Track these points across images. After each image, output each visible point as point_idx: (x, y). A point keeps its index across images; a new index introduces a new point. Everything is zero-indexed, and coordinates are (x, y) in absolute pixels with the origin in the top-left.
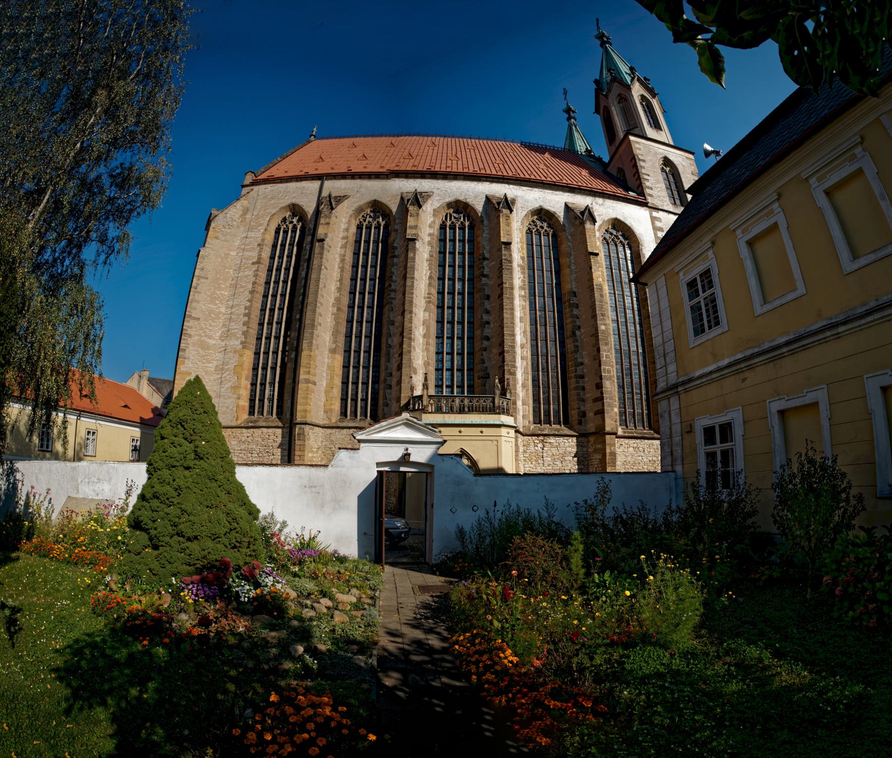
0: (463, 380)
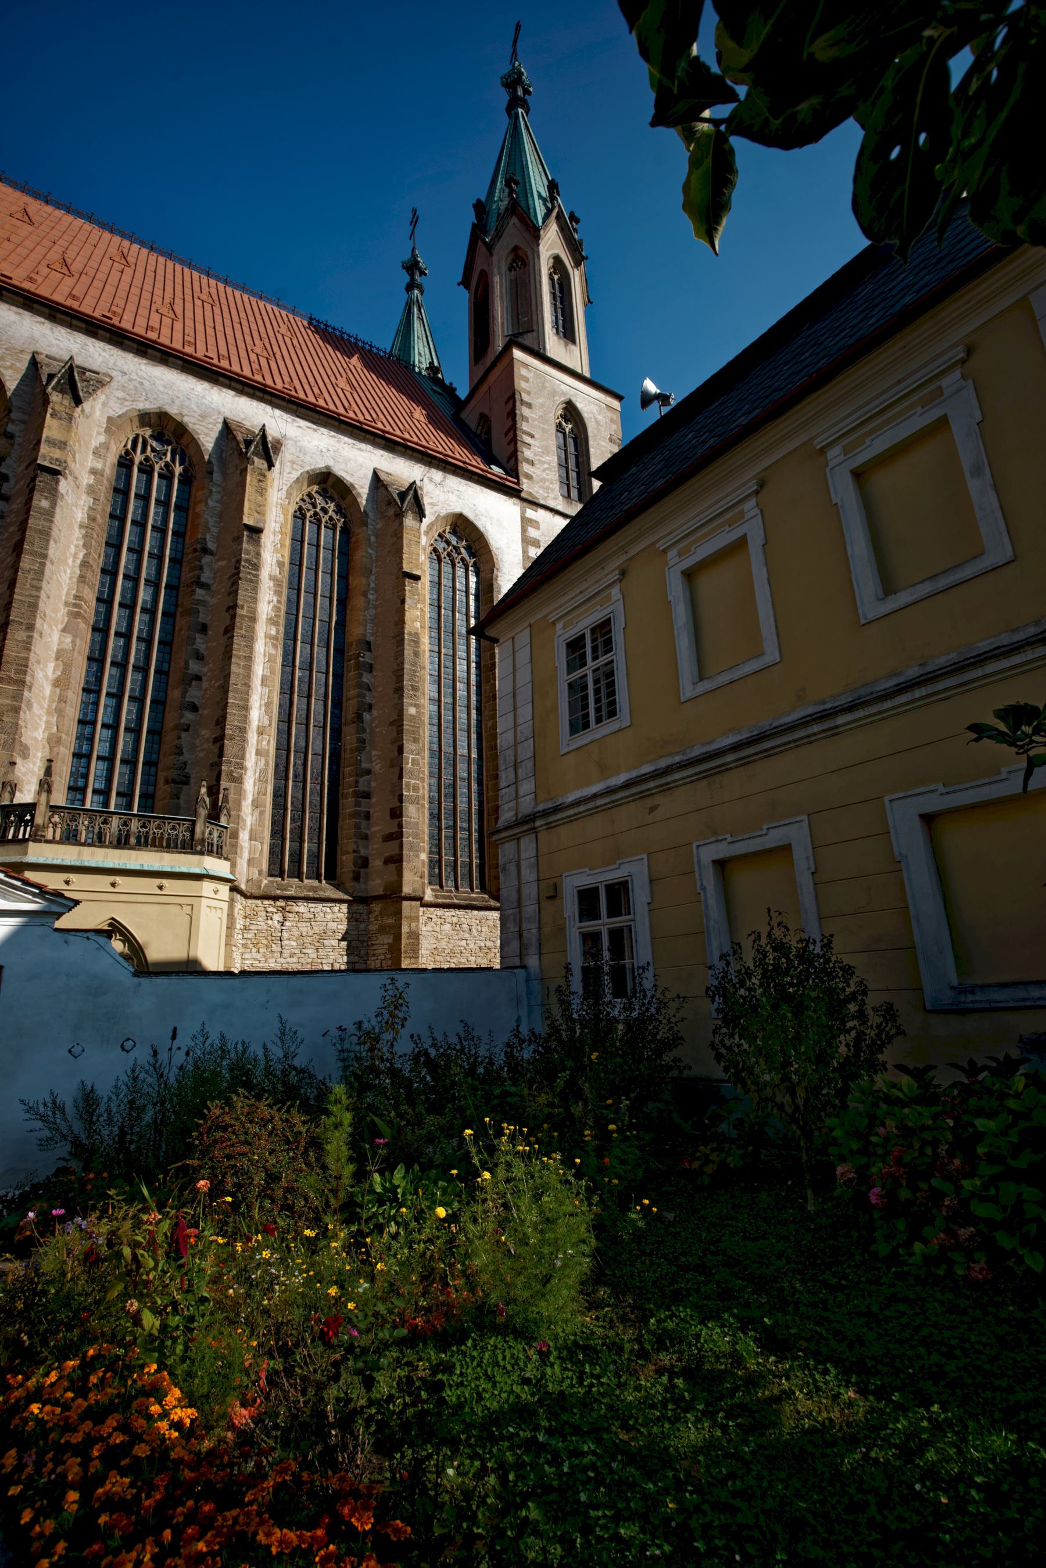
0: (132, 783)
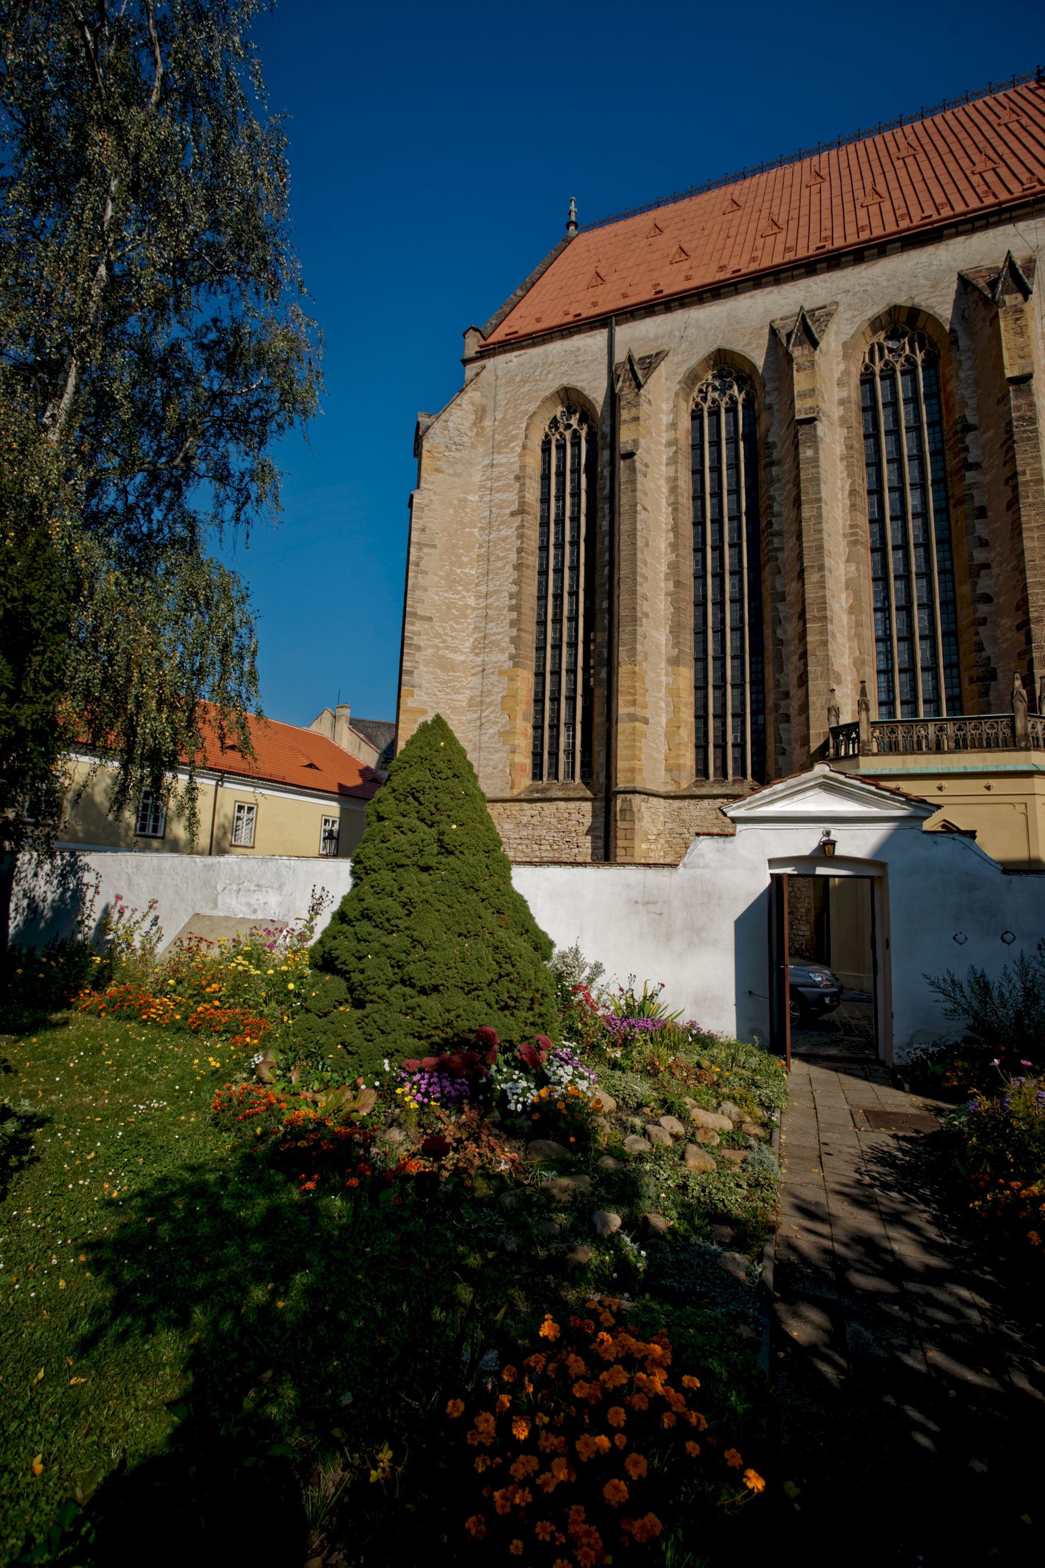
0: (936, 688)
